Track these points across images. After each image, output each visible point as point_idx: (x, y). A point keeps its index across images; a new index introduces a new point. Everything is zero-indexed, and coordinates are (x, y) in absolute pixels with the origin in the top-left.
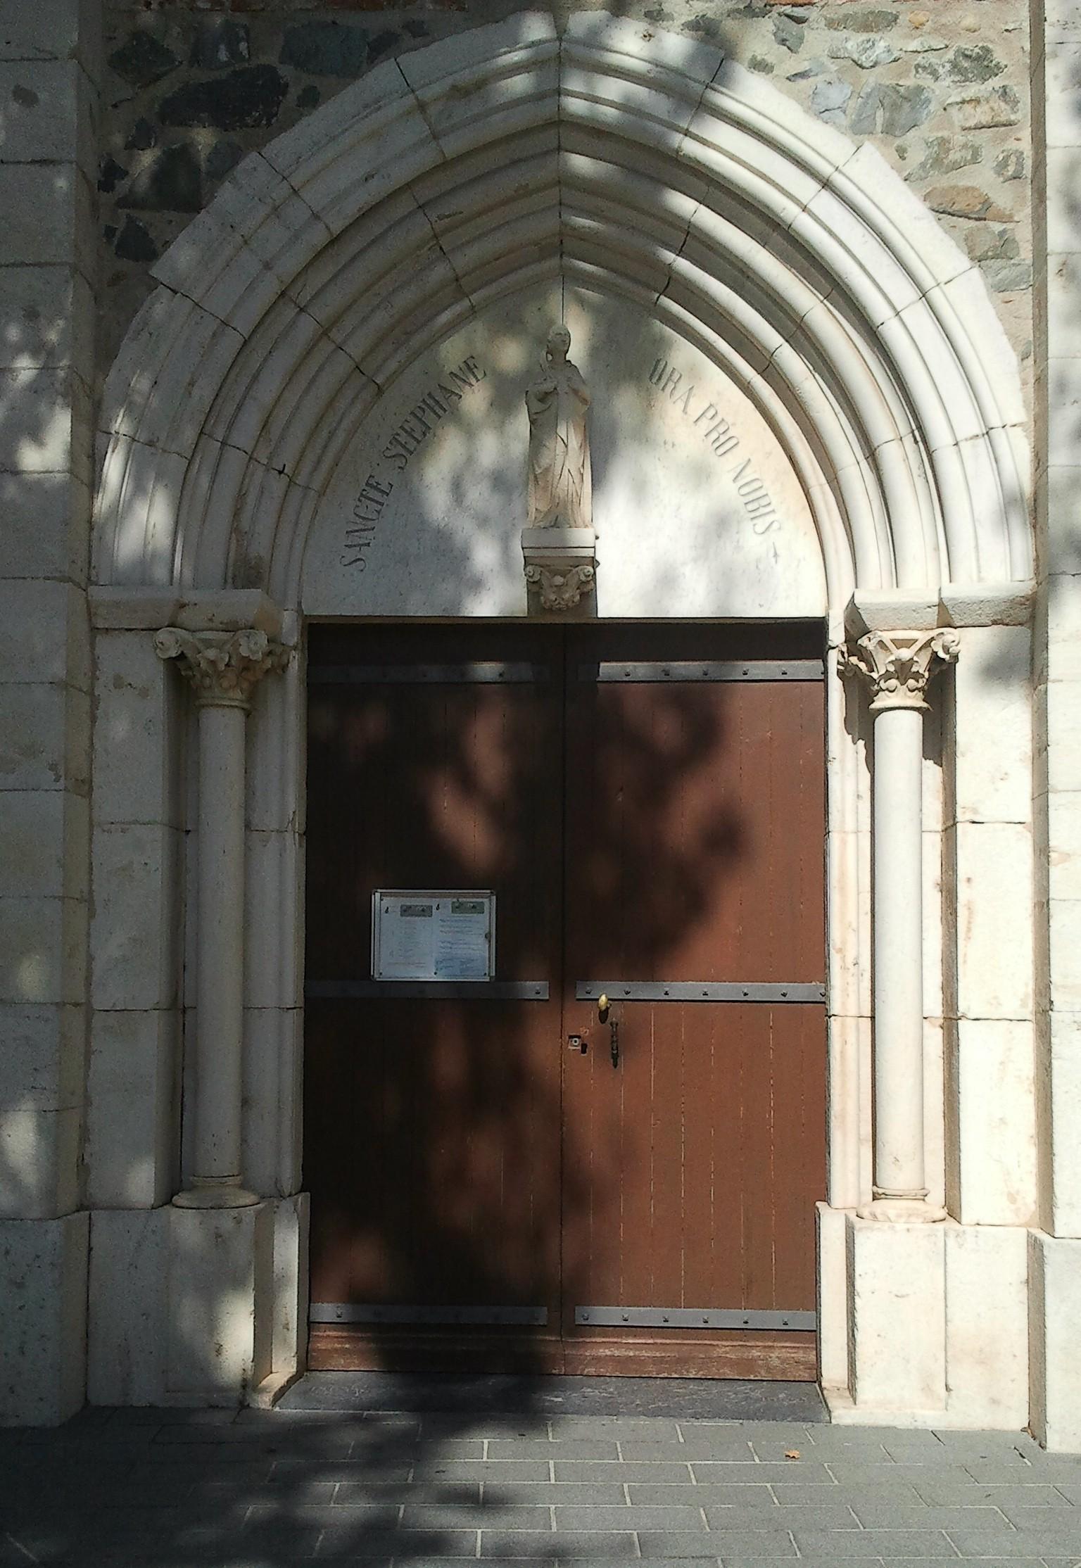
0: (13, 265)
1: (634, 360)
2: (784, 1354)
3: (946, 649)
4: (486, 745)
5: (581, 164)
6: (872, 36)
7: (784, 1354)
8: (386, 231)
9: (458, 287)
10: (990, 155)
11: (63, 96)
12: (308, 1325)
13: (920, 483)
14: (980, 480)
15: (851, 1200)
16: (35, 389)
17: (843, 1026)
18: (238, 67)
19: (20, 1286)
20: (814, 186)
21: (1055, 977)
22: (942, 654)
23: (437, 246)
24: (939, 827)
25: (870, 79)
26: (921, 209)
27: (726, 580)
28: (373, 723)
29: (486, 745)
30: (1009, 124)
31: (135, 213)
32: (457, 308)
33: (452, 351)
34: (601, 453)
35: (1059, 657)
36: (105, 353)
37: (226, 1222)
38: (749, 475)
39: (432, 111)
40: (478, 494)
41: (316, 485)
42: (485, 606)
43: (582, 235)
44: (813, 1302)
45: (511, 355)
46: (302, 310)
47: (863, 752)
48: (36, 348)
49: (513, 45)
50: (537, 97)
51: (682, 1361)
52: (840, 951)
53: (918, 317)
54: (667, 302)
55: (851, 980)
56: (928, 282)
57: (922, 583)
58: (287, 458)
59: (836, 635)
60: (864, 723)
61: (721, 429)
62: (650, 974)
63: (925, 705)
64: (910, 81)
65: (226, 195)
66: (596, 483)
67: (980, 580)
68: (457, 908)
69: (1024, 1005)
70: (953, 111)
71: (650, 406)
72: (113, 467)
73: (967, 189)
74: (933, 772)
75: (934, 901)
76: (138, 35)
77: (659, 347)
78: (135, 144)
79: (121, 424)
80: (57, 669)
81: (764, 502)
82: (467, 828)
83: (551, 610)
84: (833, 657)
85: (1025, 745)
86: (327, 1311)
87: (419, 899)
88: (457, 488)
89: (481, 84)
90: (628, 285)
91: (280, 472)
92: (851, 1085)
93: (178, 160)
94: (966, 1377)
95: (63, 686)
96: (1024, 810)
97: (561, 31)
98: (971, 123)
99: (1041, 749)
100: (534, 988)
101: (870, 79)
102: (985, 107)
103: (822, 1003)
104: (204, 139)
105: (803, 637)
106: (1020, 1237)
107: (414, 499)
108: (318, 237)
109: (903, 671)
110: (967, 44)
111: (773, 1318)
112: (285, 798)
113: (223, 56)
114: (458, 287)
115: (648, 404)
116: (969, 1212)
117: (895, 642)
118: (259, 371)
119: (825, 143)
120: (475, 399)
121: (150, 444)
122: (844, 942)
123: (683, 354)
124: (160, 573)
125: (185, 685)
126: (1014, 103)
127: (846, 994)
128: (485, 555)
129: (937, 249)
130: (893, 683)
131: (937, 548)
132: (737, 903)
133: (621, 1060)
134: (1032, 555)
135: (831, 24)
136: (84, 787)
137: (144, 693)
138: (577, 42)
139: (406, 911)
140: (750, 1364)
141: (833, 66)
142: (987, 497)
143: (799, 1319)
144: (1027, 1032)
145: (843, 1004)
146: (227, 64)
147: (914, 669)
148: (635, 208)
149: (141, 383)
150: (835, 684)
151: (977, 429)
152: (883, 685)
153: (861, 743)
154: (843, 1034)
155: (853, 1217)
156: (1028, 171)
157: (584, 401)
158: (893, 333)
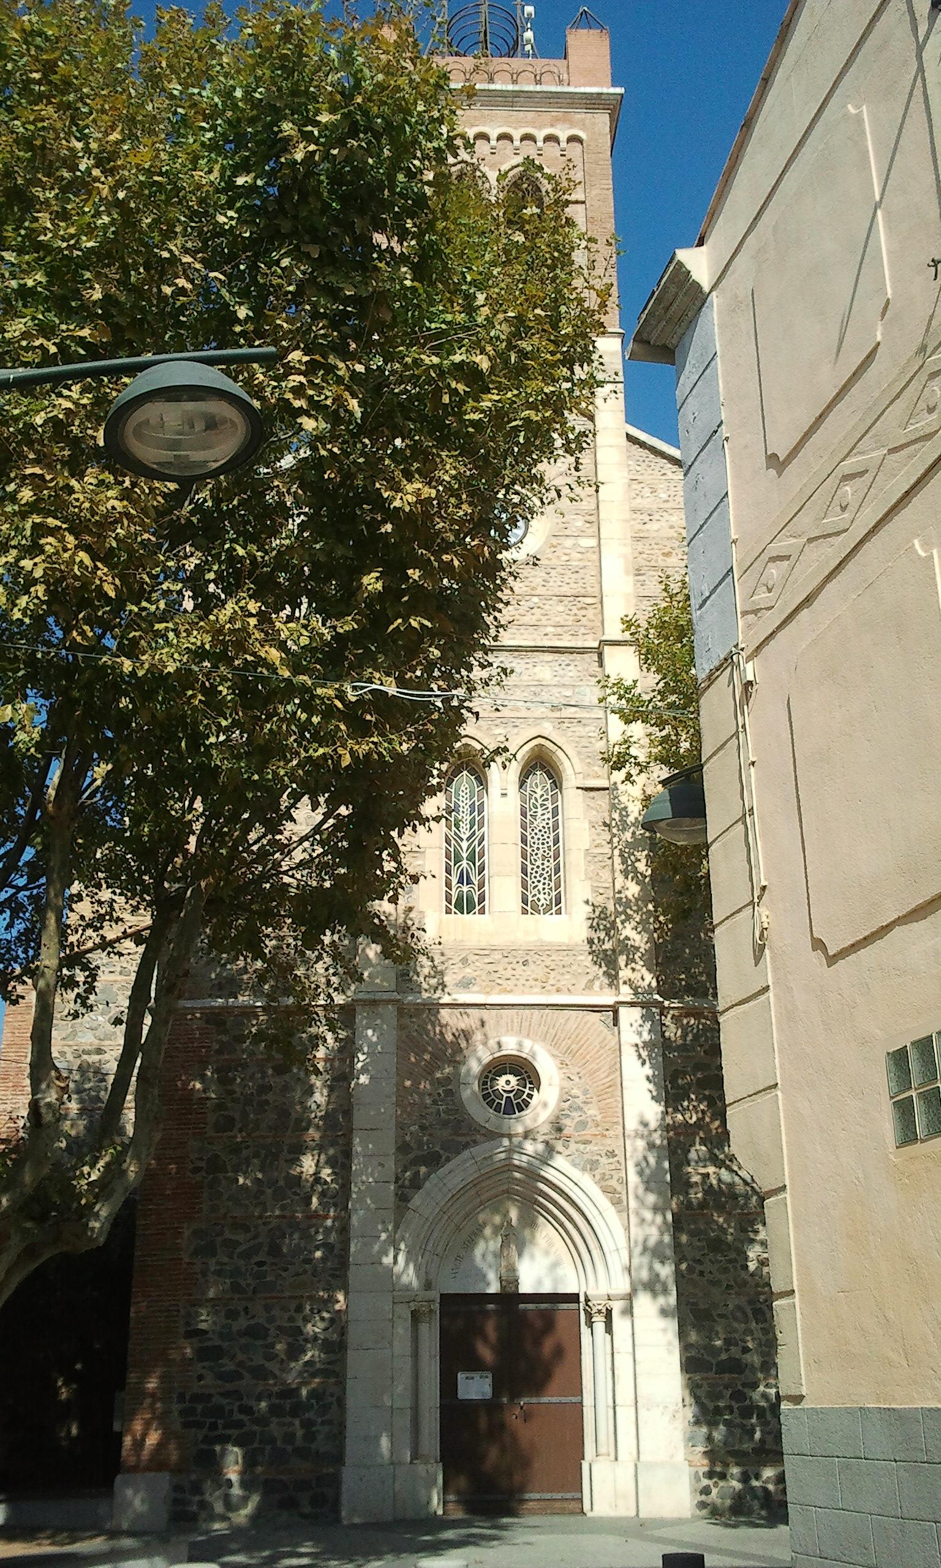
1: (528, 1222)
4: (491, 1328)
5: (517, 1175)
10: (616, 1177)
11: (391, 1164)
14: (618, 1259)
27: (556, 1281)
29: (491, 1328)
33: (482, 1217)
35: (636, 1311)
40: (490, 1258)
45: (497, 1219)
53: (599, 1218)
59: (582, 1299)
60: (590, 1324)
65: (427, 1184)
68: (481, 1377)
74: (608, 1337)
79: (402, 1246)
82: (486, 1353)
86: (451, 1497)
101: (586, 1157)
103: (581, 1403)
105: (574, 1298)
109: (599, 1312)
117: (597, 1304)
119: (575, 1173)
120: (488, 1231)
123: (541, 1219)
125: (416, 1317)
127: (588, 1401)
128: (492, 1276)
129: (603, 1201)
137: (405, 1320)
143: (578, 1495)
150: (582, 1313)
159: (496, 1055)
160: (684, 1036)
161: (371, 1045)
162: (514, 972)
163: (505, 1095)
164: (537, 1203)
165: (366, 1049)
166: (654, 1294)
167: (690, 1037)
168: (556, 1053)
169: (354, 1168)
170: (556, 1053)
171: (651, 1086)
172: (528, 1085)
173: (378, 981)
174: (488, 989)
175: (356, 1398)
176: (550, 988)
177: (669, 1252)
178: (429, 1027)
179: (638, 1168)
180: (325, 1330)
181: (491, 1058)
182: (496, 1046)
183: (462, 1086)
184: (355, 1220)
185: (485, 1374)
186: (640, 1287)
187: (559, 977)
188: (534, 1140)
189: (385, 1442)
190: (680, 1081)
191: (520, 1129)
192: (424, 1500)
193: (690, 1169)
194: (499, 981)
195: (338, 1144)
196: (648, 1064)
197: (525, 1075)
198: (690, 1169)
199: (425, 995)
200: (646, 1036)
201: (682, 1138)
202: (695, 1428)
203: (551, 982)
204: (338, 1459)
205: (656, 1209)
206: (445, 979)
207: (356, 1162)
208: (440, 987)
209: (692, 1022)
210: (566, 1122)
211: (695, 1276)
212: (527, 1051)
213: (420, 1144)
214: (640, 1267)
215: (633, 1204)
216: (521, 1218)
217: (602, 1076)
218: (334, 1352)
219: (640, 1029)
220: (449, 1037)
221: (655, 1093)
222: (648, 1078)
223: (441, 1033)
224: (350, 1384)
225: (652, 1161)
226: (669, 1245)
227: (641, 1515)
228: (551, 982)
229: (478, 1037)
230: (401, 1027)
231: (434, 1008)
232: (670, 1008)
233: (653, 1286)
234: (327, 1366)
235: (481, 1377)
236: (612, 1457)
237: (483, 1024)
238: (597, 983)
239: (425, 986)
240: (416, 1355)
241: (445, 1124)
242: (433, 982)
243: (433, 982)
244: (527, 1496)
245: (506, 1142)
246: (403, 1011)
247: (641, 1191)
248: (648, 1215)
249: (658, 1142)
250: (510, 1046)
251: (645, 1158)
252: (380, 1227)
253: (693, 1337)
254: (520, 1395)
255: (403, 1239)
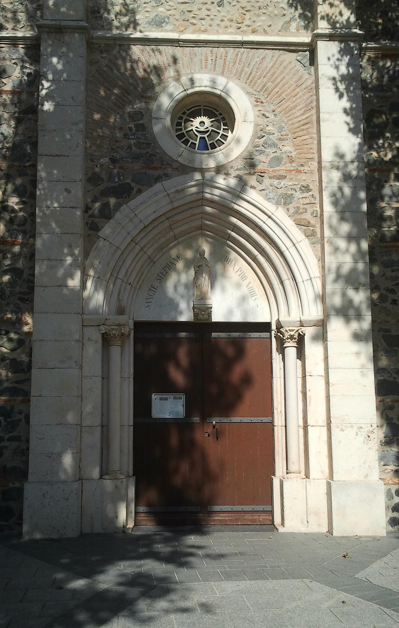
0: (65, 233)
1: (222, 257)
2: (263, 517)
3: (302, 333)
4: (183, 354)
5: (209, 209)
6: (280, 181)
7: (263, 517)
8: (158, 224)
9: (175, 238)
10: (310, 211)
11: (78, 190)
12: (136, 513)
13: (294, 290)
14: (310, 291)
15: (281, 475)
16: (71, 265)
17: (278, 428)
18: (120, 183)
19: (68, 499)
20: (267, 217)
21: (331, 415)
22: (301, 333)
23: (171, 228)
24: (301, 376)
25: (280, 191)
26: (293, 223)
27: (245, 313)
28: (153, 349)
29: (183, 354)
30: (314, 203)
31: (94, 219)
32: (174, 243)
33: (174, 253)
34: (213, 280)
35: (330, 335)
36: (86, 254)
37: (119, 483)
38: (250, 286)
39: (171, 196)
40: (181, 290)
41: (138, 287)
42: (183, 318)
43: (207, 225)
44: (272, 504)
45: (189, 254)
46: (136, 244)
47: (281, 357)
48: (72, 255)
49: (192, 180)
50: (197, 193)
51: (236, 520)
52: (276, 409)
53: (293, 250)
54: (228, 242)
55: (280, 416)
56: (295, 242)
57: (295, 316)
58: (131, 280)
59: (274, 327)
60: (282, 350)
61: (243, 274)
62: (227, 416)
63: (297, 346)
64: (290, 192)
65: (118, 216)
66: (212, 288)
67: (310, 315)
68: (174, 398)
69: (324, 422)
70: (300, 200)
71: (225, 268)
72: (89, 284)
73: (304, 219)
74: (299, 362)
75: (300, 395)
76: (94, 173)
77: (227, 253)
78: (94, 201)
79: (92, 273)
80: (77, 337)
81: (254, 292)
82: (178, 376)
83: (200, 320)
84: (273, 333)
85: (322, 357)
86: (142, 509)
87: (165, 396)
88: (175, 287)
89: (183, 190)
90: (219, 238)
91: (130, 284)
92: (280, 444)
93: (106, 205)
94: (312, 519)
95: (78, 341)
96: (322, 373)
97: (203, 177)
98: (305, 203)
99: (326, 358)
100: (196, 419)
101: (280, 191)
102: (308, 199)
104: (112, 201)
105: (265, 327)
106: (325, 482)
107: (164, 291)
108: (142, 226)
109: (292, 337)
110: (304, 184)
111: (260, 508)
112: (130, 370)
113: (117, 180)
114: (175, 238)
115: (224, 268)
116: (312, 475)
117: (290, 330)
118: (125, 259)
119: (269, 207)
120: (180, 265)
121: (98, 278)
122: (277, 407)
123: (233, 255)
124: (101, 311)
125: (106, 340)
126: (315, 199)
127: (278, 420)
128: (183, 305)
129: (297, 234)
130: (289, 340)
131: (299, 307)
132: (250, 397)
133: (219, 439)
134: (322, 309)
135: (270, 178)
136: (81, 367)
137: (96, 342)
138: (207, 180)
139: (161, 399)
140: (255, 520)
141: (271, 188)
142: (311, 295)
143: (268, 508)
144: (325, 429)
145: (278, 423)
146: (117, 182)
147: (294, 337)
148: (220, 220)
149: (96, 262)
150: (274, 340)
151: (308, 278)
152: (287, 341)
153: (281, 355)
154: (278, 431)
155: (282, 478)
156: (319, 215)
157: (209, 267)
158: (287, 254)
159: (189, 92)
160: (380, 78)
161: (55, 72)
162: (209, 13)
163: (199, 136)
164: (230, 238)
165: (50, 77)
166: (347, 319)
167: (386, 78)
168: (250, 90)
169: (38, 193)
170: (250, 90)
171: (348, 119)
172: (223, 127)
173: (63, 9)
174: (182, 29)
175: (41, 413)
176: (245, 28)
177: (364, 279)
178: (120, 62)
179: (333, 199)
180: (13, 350)
181: (182, 94)
182: (188, 83)
183: (154, 121)
184: (39, 243)
185: (178, 395)
186: (333, 313)
187: (254, 18)
188: (227, 174)
189: (68, 460)
190: (375, 120)
191: (212, 164)
192: (111, 514)
193: (383, 204)
194: (194, 21)
195: (27, 174)
196: (345, 98)
197: (220, 117)
198: (383, 204)
199: (115, 32)
200: (343, 70)
201: (376, 175)
202: (386, 448)
203: (247, 22)
204: (23, 474)
205: (350, 238)
206: (138, 17)
207: (40, 186)
208: (132, 26)
209: (389, 64)
210: (259, 158)
211: (388, 305)
212: (221, 88)
213: (111, 178)
214: (333, 293)
215: (327, 233)
216: (212, 253)
217: (298, 114)
218: (22, 371)
219: (337, 63)
220: (140, 73)
221: (352, 126)
222: (345, 111)
223: (133, 69)
224: (34, 401)
225: (347, 191)
226: (364, 273)
227: (336, 533)
228: (247, 22)
229: (170, 73)
230: (91, 63)
231: (125, 43)
232: (367, 49)
233: (347, 312)
234: (14, 385)
235: (174, 398)
236: (303, 474)
237: (175, 60)
238: (294, 25)
239: (116, 23)
240: (106, 377)
241: (136, 158)
242: (125, 19)
243: (125, 19)
244: (217, 508)
245: (198, 176)
246: (91, 45)
247: (335, 221)
248: (342, 244)
249: (354, 173)
250: (203, 82)
251: (340, 189)
252: (66, 251)
253: (384, 362)
254: (211, 416)
255: (92, 266)
